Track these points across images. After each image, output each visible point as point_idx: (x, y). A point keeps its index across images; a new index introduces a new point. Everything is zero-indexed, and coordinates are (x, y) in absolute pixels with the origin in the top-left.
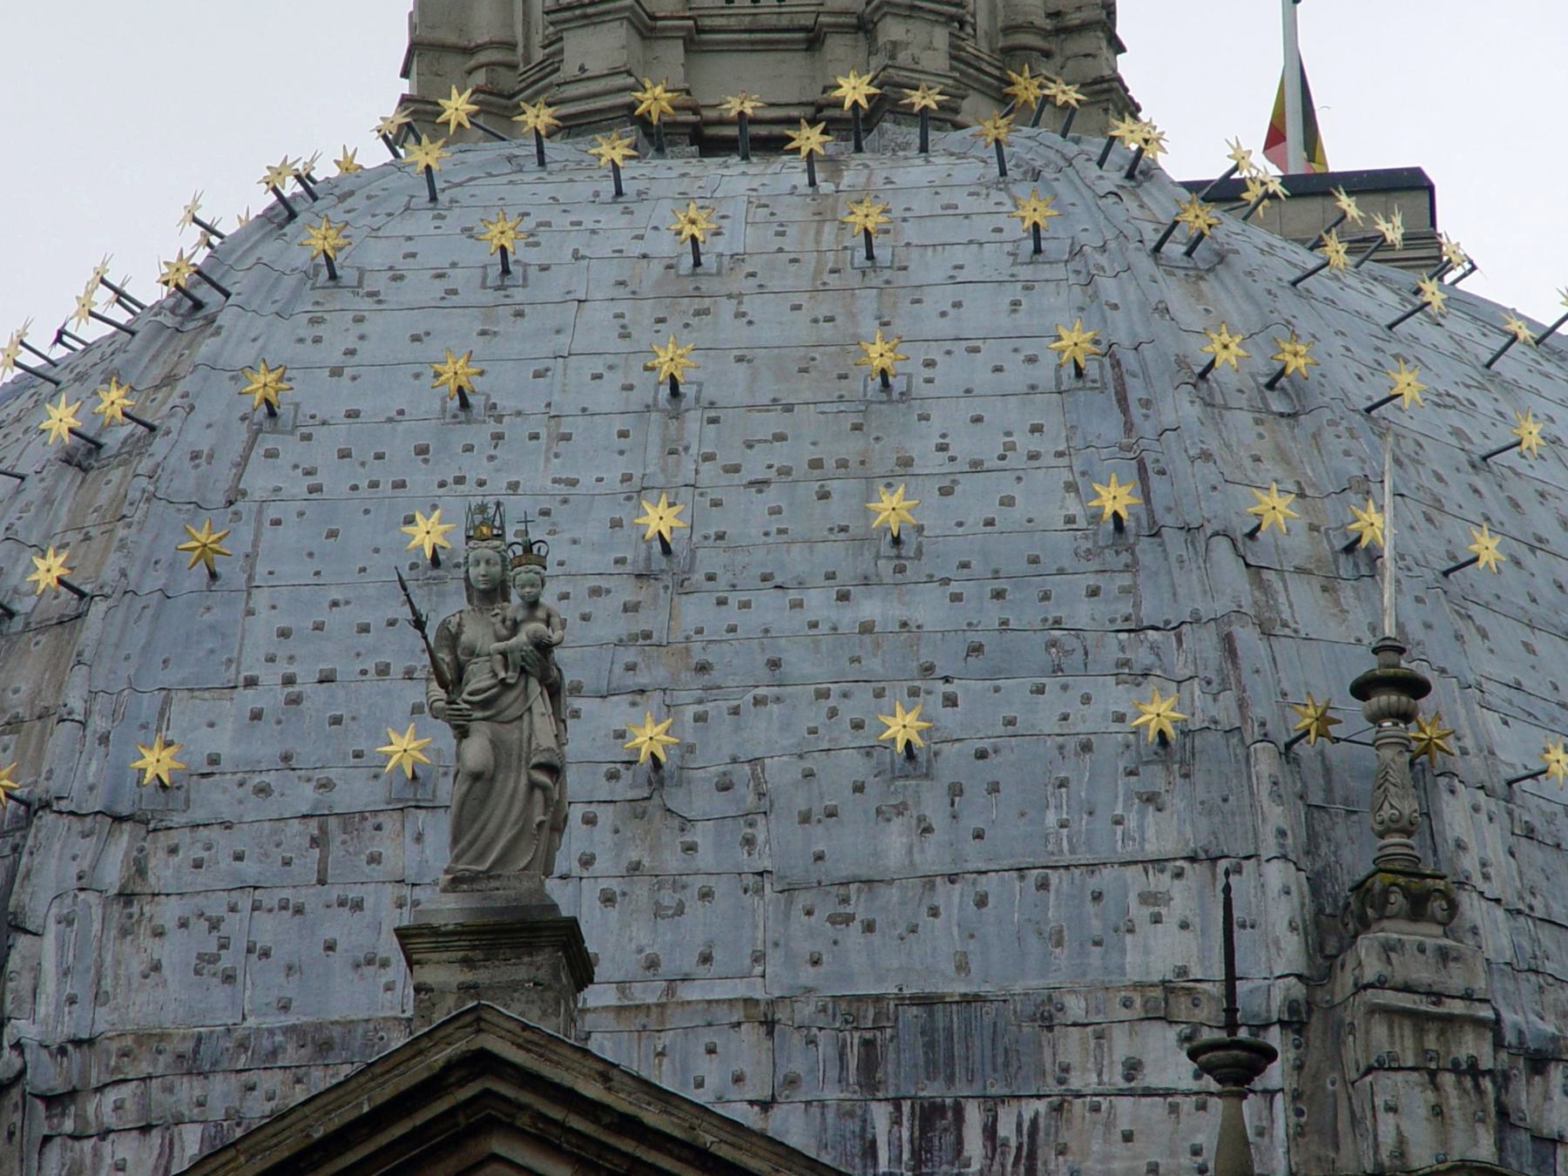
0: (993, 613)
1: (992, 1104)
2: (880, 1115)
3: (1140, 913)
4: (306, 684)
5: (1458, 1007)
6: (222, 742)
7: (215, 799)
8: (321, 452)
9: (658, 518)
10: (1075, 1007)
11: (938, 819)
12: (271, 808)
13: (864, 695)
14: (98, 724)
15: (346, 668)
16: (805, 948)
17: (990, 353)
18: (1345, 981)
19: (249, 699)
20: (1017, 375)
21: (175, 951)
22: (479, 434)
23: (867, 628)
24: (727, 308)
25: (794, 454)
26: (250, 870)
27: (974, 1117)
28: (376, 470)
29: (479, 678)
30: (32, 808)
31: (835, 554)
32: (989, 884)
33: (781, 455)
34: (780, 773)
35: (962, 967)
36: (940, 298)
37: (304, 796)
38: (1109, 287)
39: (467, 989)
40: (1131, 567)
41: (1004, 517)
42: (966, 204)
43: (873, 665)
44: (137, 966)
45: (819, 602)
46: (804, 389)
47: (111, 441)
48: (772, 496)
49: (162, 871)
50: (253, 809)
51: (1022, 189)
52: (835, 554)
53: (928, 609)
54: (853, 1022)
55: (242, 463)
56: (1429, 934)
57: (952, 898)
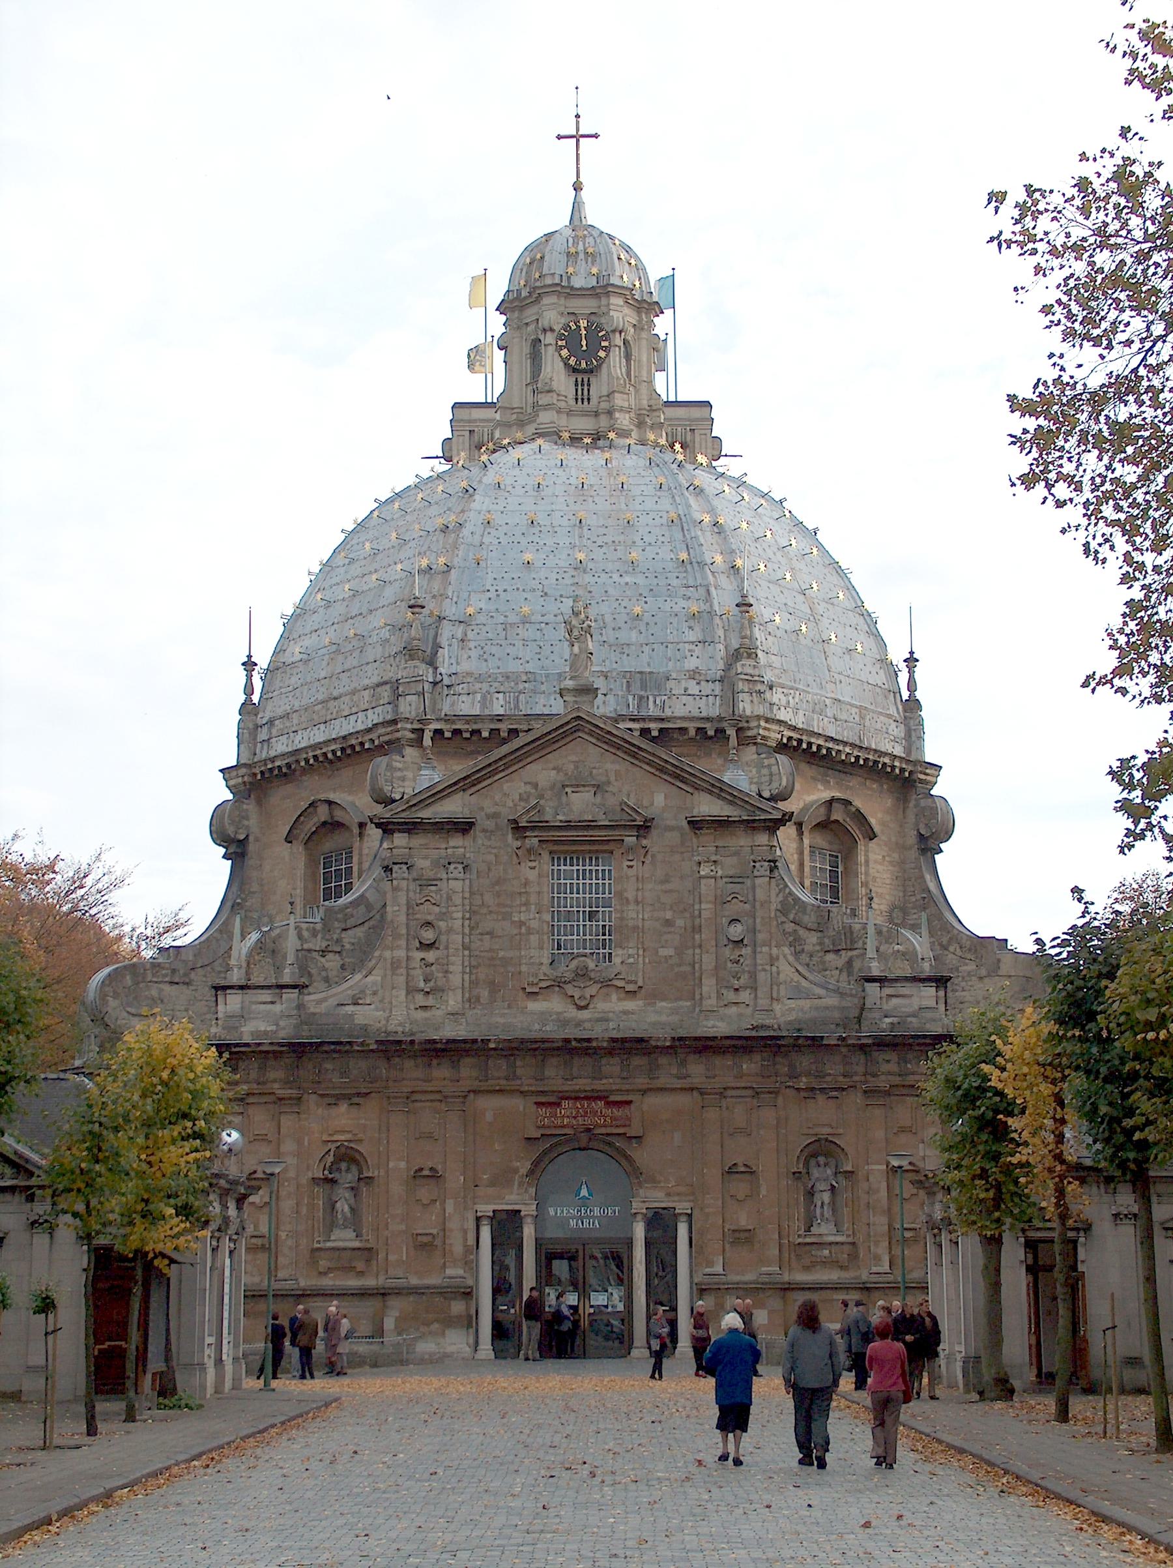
0: (655, 581)
1: (655, 697)
2: (630, 698)
3: (688, 654)
4: (501, 592)
5: (756, 678)
6: (482, 605)
7: (481, 619)
8: (500, 534)
9: (581, 556)
10: (674, 675)
11: (643, 631)
12: (494, 621)
13: (626, 600)
14: (455, 599)
15: (509, 588)
16: (614, 660)
17: (652, 515)
18: (733, 672)
19: (489, 595)
20: (658, 521)
21: (474, 654)
22: (536, 530)
23: (627, 584)
24: (591, 500)
25: (608, 539)
26: (490, 635)
27: (651, 699)
28: (513, 538)
29: (576, 633)
30: (441, 619)
31: (618, 565)
32: (655, 646)
33: (605, 539)
34: (608, 618)
35: (649, 665)
36: (639, 499)
37: (502, 619)
38: (677, 498)
39: (576, 702)
40: (686, 572)
41: (656, 557)
42: (643, 473)
43: (628, 593)
44: (466, 656)
45: (616, 577)
46: (610, 522)
47: (451, 527)
48: (604, 550)
49: (470, 635)
50: (490, 621)
51: (656, 469)
52: (618, 565)
53: (640, 580)
54: (624, 677)
55: (482, 536)
56: (753, 663)
57: (646, 649)
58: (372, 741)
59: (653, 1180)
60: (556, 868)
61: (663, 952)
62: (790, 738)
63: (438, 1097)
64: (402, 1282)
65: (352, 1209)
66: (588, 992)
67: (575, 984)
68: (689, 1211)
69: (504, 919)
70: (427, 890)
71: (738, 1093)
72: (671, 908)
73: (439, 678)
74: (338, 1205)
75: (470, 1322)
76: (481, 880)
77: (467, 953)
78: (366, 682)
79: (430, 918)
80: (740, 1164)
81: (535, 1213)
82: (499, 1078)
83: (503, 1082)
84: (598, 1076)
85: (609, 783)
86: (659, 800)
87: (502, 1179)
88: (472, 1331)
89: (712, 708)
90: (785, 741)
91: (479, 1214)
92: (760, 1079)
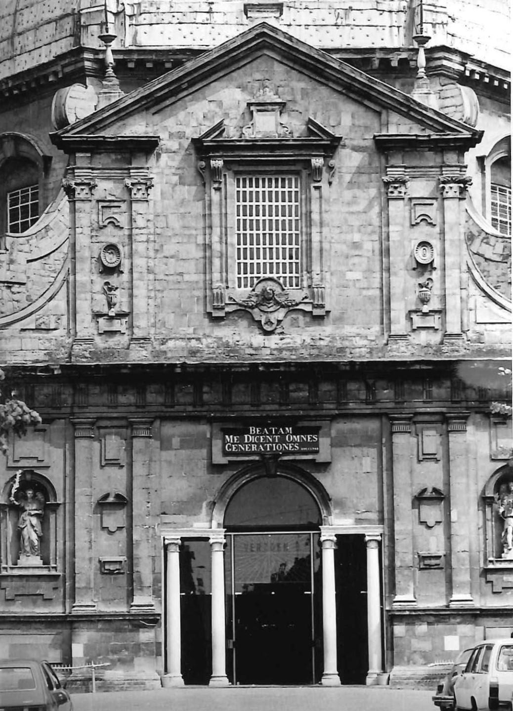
58: (55, 74)
59: (341, 504)
60: (241, 189)
61: (350, 276)
62: (473, 72)
63: (123, 423)
64: (89, 611)
65: (41, 539)
66: (273, 317)
67: (263, 308)
68: (379, 538)
69: (188, 242)
70: (109, 213)
71: (426, 418)
72: (359, 231)
73: (120, 8)
74: (25, 532)
75: (160, 650)
76: (166, 202)
77: (151, 277)
78: (47, 16)
79: (114, 241)
80: (430, 490)
81: (224, 541)
82: (185, 404)
83: (190, 408)
84: (38, 588)
85: (294, 101)
86: (346, 120)
87: (187, 507)
88: (15, 670)
89: (396, 40)
90: (467, 73)
91: (167, 542)
92: (449, 404)
